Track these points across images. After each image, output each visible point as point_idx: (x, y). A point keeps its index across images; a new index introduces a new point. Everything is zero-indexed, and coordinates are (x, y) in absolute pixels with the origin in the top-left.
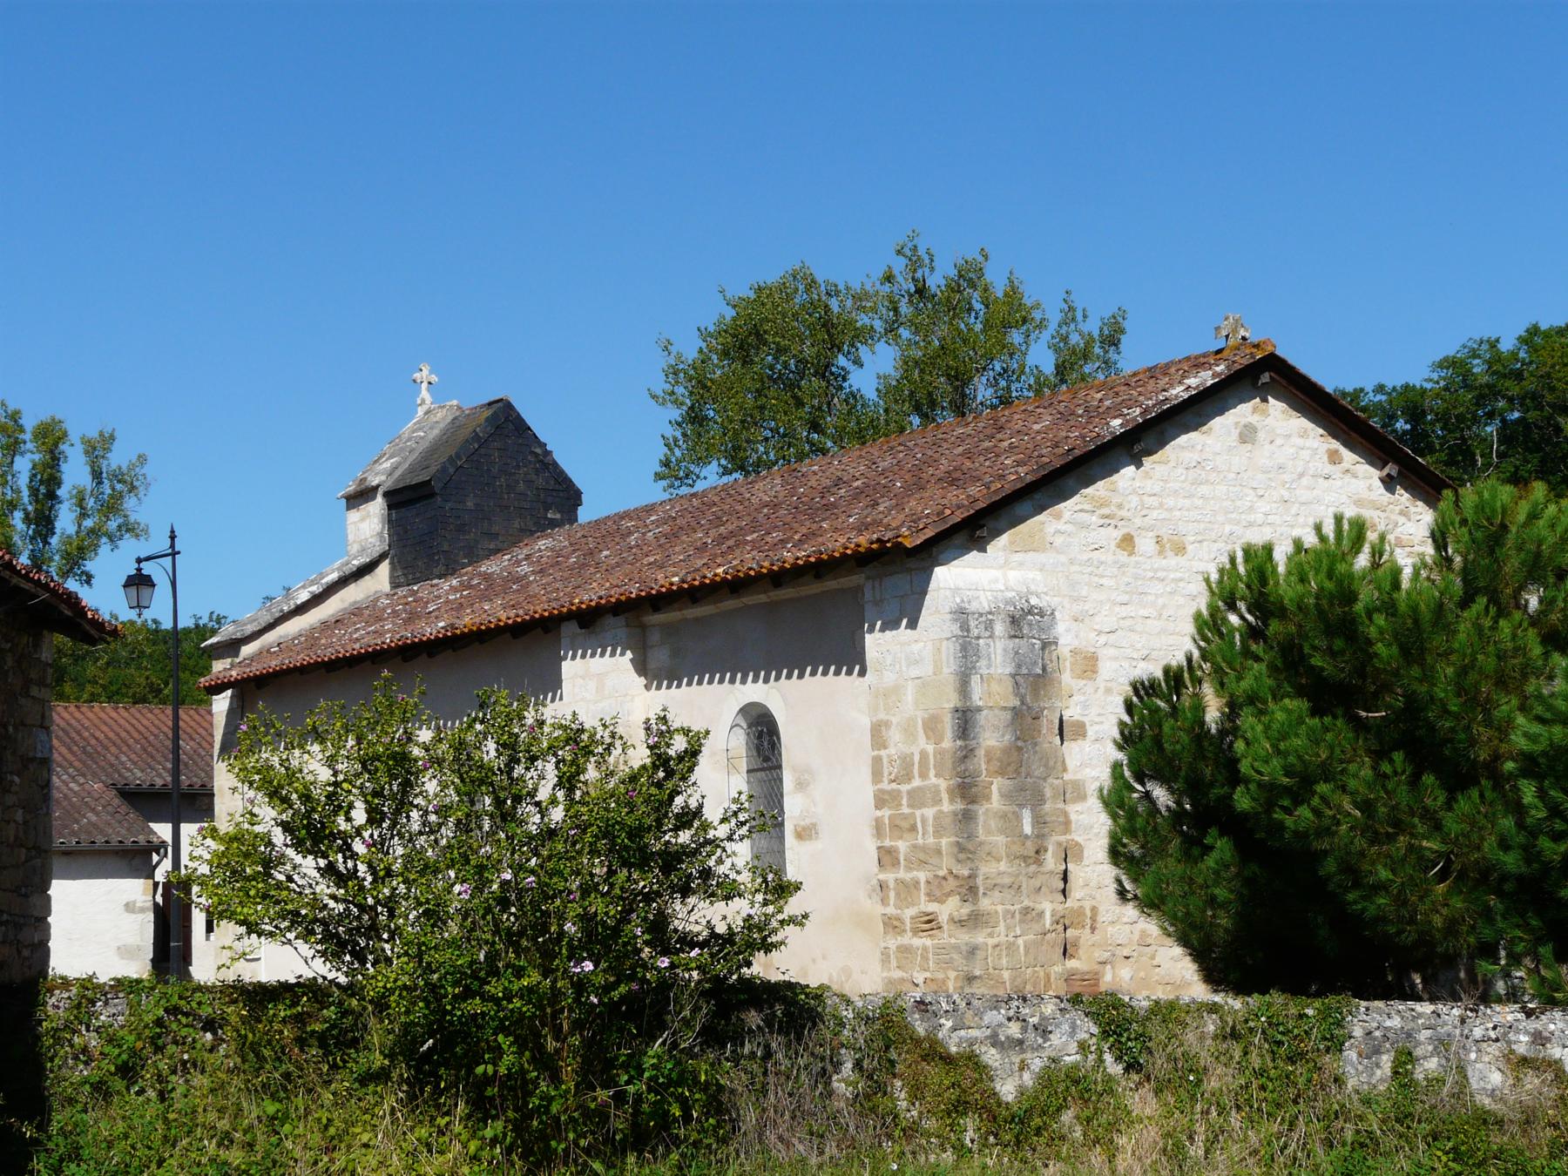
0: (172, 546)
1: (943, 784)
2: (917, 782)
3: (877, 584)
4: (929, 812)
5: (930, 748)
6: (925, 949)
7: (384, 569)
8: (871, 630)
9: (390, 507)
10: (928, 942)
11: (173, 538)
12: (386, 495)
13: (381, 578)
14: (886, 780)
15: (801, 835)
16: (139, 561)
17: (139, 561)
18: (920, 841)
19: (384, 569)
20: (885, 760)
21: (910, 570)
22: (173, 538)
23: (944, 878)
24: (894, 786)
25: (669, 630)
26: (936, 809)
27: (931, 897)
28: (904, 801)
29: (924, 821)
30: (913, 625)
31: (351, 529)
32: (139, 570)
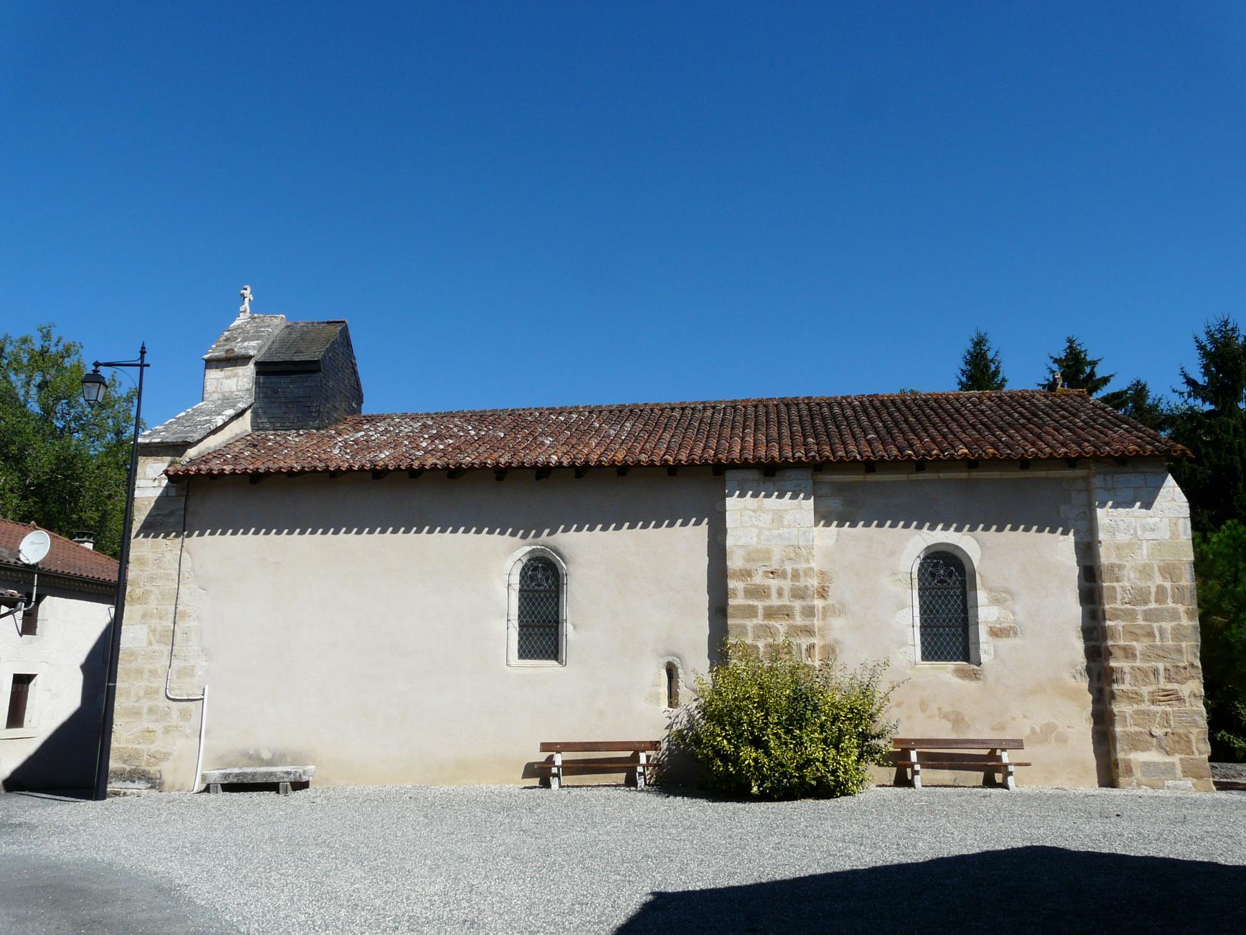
0: (142, 358)
1: (1181, 608)
2: (1153, 605)
3: (1108, 477)
4: (1168, 626)
5: (1168, 585)
6: (1167, 714)
7: (248, 414)
8: (1103, 505)
9: (257, 373)
10: (1168, 709)
11: (143, 353)
12: (257, 364)
13: (244, 425)
14: (1118, 602)
15: (995, 633)
16: (97, 364)
17: (97, 364)
18: (1158, 643)
19: (248, 414)
20: (1119, 590)
21: (1143, 473)
22: (143, 353)
23: (1185, 668)
24: (1128, 606)
25: (840, 488)
26: (1173, 624)
27: (1169, 679)
28: (1140, 617)
29: (1161, 631)
30: (1147, 505)
31: (210, 387)
32: (96, 371)
